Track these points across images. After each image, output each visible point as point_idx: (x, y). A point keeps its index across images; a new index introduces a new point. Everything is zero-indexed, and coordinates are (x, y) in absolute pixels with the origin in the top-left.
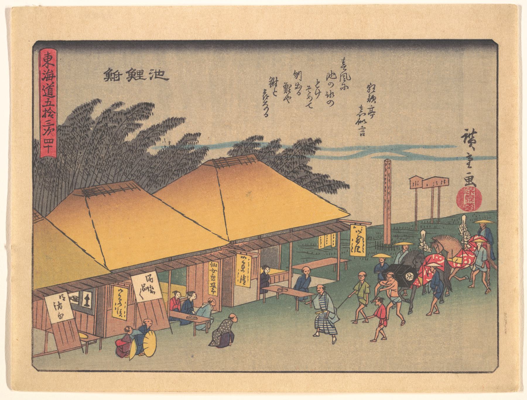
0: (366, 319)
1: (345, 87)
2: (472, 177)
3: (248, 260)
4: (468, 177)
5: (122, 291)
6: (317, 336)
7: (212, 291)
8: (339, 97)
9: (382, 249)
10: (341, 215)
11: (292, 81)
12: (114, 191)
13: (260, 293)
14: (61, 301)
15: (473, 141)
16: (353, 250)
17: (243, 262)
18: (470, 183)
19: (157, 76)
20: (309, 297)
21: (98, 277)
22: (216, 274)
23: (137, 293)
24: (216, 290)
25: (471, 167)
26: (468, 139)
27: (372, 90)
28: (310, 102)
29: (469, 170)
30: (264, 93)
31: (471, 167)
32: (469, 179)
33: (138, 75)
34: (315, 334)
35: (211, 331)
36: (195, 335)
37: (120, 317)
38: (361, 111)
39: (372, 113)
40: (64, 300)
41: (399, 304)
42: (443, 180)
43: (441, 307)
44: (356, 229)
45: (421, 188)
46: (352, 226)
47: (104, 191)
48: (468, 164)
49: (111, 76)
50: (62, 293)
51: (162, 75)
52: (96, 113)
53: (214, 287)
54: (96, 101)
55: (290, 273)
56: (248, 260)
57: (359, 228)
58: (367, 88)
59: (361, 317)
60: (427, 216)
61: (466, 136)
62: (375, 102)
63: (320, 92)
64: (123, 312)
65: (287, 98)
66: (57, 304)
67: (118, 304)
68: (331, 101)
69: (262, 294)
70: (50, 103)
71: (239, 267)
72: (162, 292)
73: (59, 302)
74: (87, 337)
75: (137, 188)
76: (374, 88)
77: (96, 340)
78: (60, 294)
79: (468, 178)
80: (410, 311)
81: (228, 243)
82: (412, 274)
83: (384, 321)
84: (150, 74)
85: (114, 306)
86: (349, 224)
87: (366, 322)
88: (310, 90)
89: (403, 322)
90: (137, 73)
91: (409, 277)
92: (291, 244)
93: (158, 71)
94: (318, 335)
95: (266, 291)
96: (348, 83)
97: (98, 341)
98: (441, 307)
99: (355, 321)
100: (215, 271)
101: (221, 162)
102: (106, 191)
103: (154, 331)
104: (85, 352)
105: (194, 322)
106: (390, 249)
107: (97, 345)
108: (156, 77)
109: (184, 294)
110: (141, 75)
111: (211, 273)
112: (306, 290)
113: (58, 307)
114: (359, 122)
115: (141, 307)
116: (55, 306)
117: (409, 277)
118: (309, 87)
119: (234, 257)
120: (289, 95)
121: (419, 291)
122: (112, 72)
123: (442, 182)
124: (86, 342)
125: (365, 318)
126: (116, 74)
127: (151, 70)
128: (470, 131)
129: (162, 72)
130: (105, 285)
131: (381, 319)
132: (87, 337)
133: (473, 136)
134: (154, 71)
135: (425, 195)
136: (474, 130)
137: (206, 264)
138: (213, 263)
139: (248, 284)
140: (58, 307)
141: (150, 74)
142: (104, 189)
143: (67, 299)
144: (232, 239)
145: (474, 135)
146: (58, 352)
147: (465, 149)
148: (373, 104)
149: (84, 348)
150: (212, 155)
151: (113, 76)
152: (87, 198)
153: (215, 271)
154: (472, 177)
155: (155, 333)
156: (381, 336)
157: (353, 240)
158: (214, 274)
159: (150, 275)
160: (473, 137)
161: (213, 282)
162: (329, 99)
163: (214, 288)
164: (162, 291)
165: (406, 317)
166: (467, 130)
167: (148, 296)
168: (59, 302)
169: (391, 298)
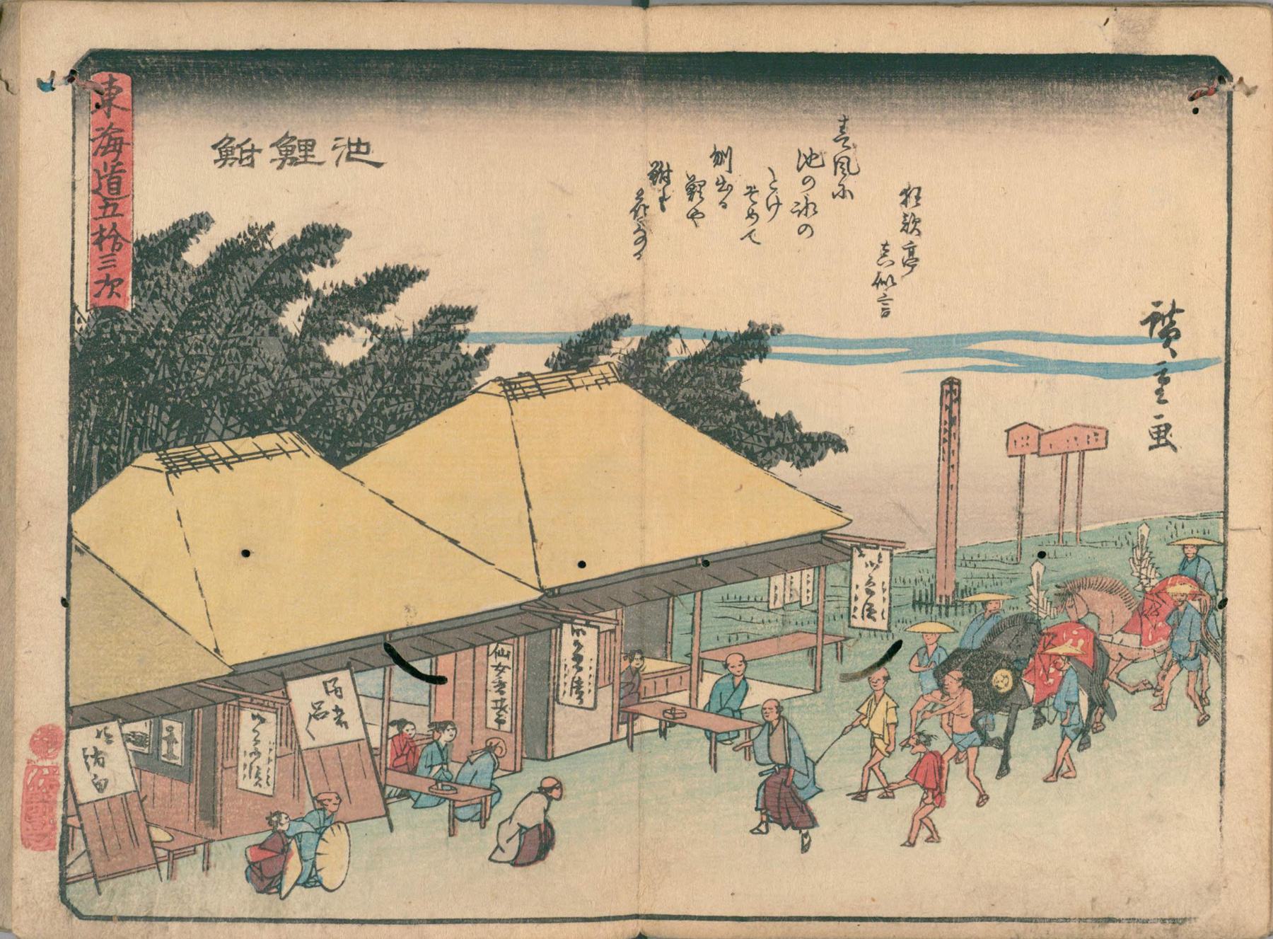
0: (888, 792)
1: (843, 193)
2: (1168, 427)
3: (589, 639)
4: (1159, 427)
5: (263, 721)
6: (761, 832)
7: (496, 721)
8: (829, 213)
9: (927, 612)
10: (824, 520)
11: (708, 172)
12: (239, 458)
13: (619, 723)
14: (101, 744)
15: (1173, 334)
16: (858, 614)
17: (576, 643)
18: (1163, 441)
19: (352, 156)
20: (742, 733)
21: (202, 684)
22: (507, 676)
23: (301, 723)
24: (507, 717)
25: (1166, 402)
26: (1159, 327)
27: (912, 201)
28: (753, 227)
29: (1161, 409)
30: (637, 199)
31: (1166, 402)
32: (1159, 432)
33: (300, 150)
34: (757, 828)
35: (493, 823)
36: (452, 833)
37: (257, 789)
38: (884, 256)
39: (911, 262)
40: (109, 742)
41: (972, 751)
42: (1090, 432)
43: (1081, 759)
44: (867, 559)
45: (1036, 456)
46: (856, 554)
47: (216, 457)
48: (1159, 392)
49: (232, 154)
50: (105, 725)
51: (367, 153)
52: (197, 254)
53: (502, 709)
54: (201, 222)
55: (695, 673)
56: (589, 639)
57: (871, 555)
58: (901, 194)
59: (874, 783)
60: (461, 655)
61: (1153, 319)
62: (919, 234)
63: (779, 204)
64: (263, 775)
65: (694, 215)
66: (90, 752)
67: (251, 754)
68: (807, 226)
69: (625, 726)
70: (115, 210)
71: (568, 651)
72: (364, 724)
73: (95, 748)
74: (169, 838)
75: (300, 449)
76: (918, 198)
77: (195, 846)
78: (100, 727)
79: (1156, 430)
80: (1004, 769)
81: (539, 594)
82: (1008, 673)
83: (936, 792)
84: (335, 148)
85: (242, 760)
86: (849, 544)
87: (888, 797)
88: (755, 197)
89: (983, 799)
90: (300, 146)
91: (1002, 679)
92: (522, 639)
93: (354, 141)
94: (764, 830)
95: (636, 715)
96: (850, 183)
97: (200, 849)
98: (1081, 759)
99: (861, 795)
100: (506, 670)
101: (523, 385)
102: (220, 459)
103: (345, 824)
104: (164, 878)
105: (450, 800)
106: (952, 610)
107: (197, 860)
108: (349, 159)
109: (423, 727)
110: (309, 153)
111: (492, 674)
112: (737, 713)
113: (93, 760)
114: (878, 282)
115: (310, 758)
116: (86, 757)
117: (1002, 679)
118: (751, 191)
119: (554, 631)
120: (699, 208)
121: (1026, 717)
122: (234, 144)
123: (1089, 437)
124: (169, 851)
125: (884, 788)
126: (245, 147)
127: (336, 139)
128: (1165, 309)
129: (364, 144)
130: (456, 651)
131: (928, 789)
132: (169, 838)
133: (1174, 319)
134: (345, 142)
135: (1044, 471)
136: (1174, 304)
137: (481, 651)
138: (501, 646)
139: (588, 700)
140: (93, 760)
141: (335, 148)
142: (216, 453)
143: (118, 740)
144: (548, 583)
145: (1176, 317)
146: (94, 876)
147: (1155, 353)
148: (912, 237)
149: (164, 866)
150: (504, 363)
151: (237, 153)
152: (171, 476)
153: (504, 667)
154: (1168, 427)
155: (347, 830)
156: (925, 833)
157: (857, 587)
158: (502, 675)
159: (336, 679)
160: (1173, 323)
161: (498, 697)
162: (803, 220)
163: (502, 713)
164: (366, 721)
165: (991, 785)
166: (1158, 304)
167: (327, 731)
168: (95, 748)
169: (955, 736)
